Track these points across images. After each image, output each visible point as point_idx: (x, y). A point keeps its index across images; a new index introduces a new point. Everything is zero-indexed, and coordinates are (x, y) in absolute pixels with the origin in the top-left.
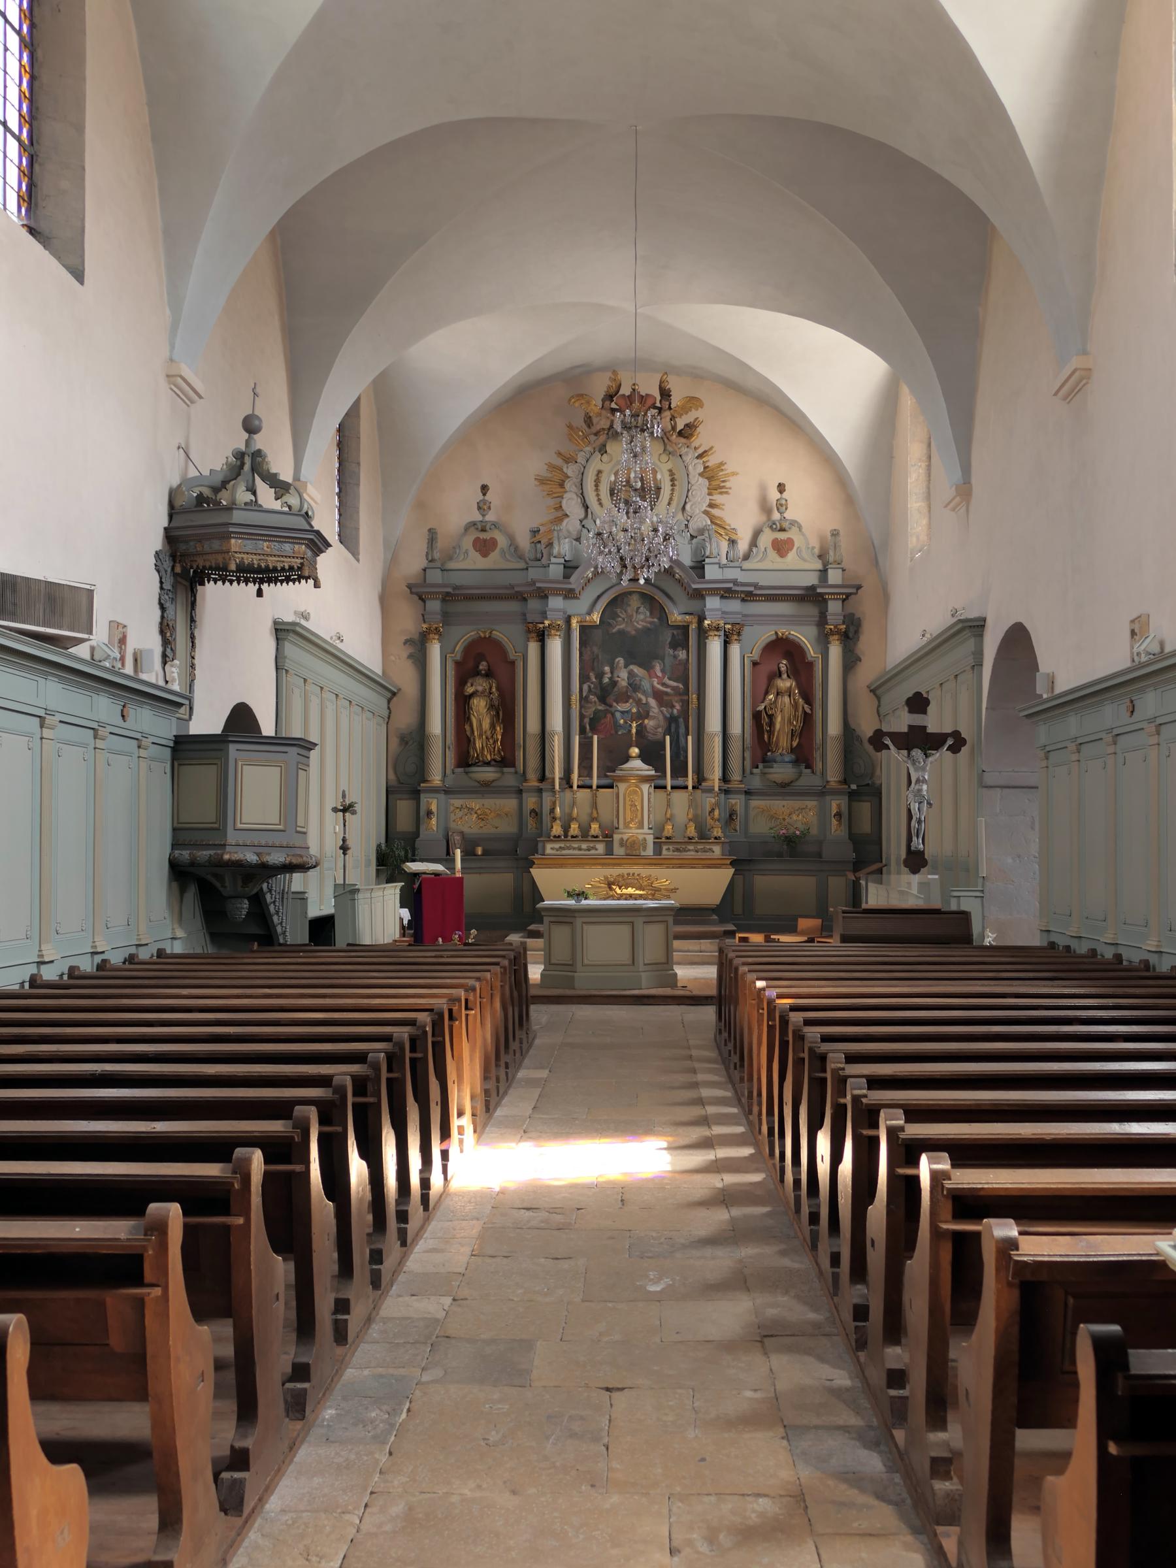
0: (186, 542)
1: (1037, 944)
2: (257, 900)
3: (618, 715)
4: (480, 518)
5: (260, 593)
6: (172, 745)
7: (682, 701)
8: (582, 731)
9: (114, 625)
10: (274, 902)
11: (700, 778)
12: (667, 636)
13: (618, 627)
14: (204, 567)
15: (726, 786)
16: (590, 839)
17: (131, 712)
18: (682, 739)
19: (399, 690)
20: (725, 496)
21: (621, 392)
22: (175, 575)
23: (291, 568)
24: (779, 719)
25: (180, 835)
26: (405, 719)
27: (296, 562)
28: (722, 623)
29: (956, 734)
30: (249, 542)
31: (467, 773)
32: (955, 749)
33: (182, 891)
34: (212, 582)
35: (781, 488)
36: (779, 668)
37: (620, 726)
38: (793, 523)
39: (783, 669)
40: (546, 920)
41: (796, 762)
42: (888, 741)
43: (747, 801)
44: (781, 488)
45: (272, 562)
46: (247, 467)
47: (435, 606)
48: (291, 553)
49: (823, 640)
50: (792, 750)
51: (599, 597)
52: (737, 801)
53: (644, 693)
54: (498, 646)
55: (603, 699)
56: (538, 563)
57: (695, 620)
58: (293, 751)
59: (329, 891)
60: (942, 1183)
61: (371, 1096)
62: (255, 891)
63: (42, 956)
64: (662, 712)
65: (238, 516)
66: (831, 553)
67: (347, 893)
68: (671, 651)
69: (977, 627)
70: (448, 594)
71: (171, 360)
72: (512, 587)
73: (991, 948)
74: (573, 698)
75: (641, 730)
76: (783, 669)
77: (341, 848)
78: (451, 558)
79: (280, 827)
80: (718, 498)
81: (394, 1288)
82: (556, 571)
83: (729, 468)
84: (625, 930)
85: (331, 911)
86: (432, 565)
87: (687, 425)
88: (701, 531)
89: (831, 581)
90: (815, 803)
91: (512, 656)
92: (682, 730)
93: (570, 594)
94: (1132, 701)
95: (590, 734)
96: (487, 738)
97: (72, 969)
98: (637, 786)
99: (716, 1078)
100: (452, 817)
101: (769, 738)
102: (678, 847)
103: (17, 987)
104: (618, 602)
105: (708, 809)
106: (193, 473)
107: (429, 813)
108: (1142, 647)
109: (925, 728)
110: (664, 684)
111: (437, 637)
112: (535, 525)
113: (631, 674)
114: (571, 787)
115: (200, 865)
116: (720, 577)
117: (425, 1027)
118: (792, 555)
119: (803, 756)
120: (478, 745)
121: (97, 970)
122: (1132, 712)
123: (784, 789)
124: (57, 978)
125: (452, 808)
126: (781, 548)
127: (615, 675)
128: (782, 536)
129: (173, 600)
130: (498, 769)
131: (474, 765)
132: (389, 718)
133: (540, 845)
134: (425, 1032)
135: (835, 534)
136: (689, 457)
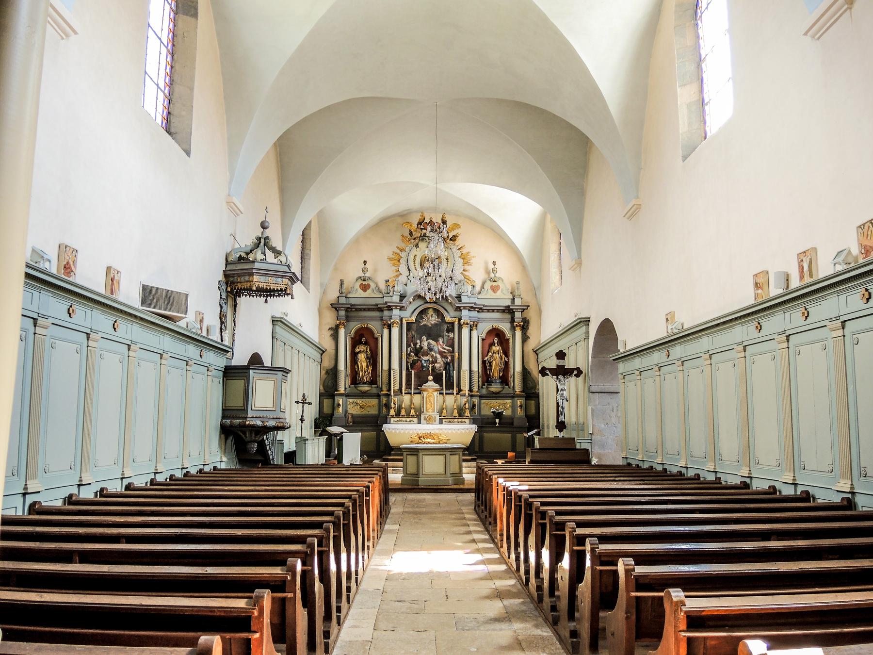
0: (233, 277)
1: (621, 464)
2: (262, 444)
3: (423, 362)
4: (363, 275)
5: (266, 301)
6: (223, 370)
7: (452, 355)
8: (407, 368)
9: (198, 313)
10: (269, 444)
11: (460, 390)
12: (445, 327)
13: (423, 323)
14: (241, 288)
15: (471, 394)
16: (410, 417)
17: (204, 354)
18: (451, 372)
19: (326, 350)
20: (470, 266)
21: (425, 221)
22: (228, 292)
23: (281, 290)
24: (494, 364)
25: (226, 412)
26: (328, 363)
27: (283, 287)
28: (469, 321)
29: (578, 369)
30: (262, 277)
31: (356, 387)
32: (578, 376)
33: (226, 439)
34: (244, 296)
35: (494, 263)
36: (494, 341)
37: (424, 367)
38: (500, 278)
39: (496, 342)
40: (405, 454)
41: (502, 383)
42: (548, 372)
43: (480, 400)
44: (494, 263)
45: (272, 287)
46: (262, 244)
47: (342, 313)
48: (281, 283)
49: (513, 329)
50: (500, 378)
51: (415, 310)
52: (476, 400)
53: (435, 352)
54: (370, 331)
55: (416, 355)
56: (388, 295)
57: (457, 320)
58: (280, 373)
59: (294, 440)
60: (681, 608)
61: (325, 547)
62: (261, 439)
63: (157, 470)
64: (442, 360)
65: (257, 265)
66: (516, 291)
67: (301, 441)
68: (447, 334)
69: (586, 321)
70: (348, 308)
71: (229, 195)
72: (377, 305)
73: (595, 466)
74: (403, 354)
75: (434, 368)
76: (496, 342)
77: (300, 420)
78: (350, 293)
79: (273, 409)
80: (467, 267)
81: (335, 650)
82: (396, 299)
83: (472, 254)
84: (442, 458)
85: (295, 449)
86: (342, 295)
87: (454, 236)
88: (460, 282)
89: (516, 303)
90: (510, 401)
91: (376, 335)
92: (451, 369)
93: (402, 308)
94: (668, 351)
95: (411, 370)
96: (365, 371)
97: (171, 476)
98: (432, 393)
99: (479, 529)
100: (349, 407)
101: (489, 372)
102: (450, 420)
103: (144, 485)
104: (423, 312)
105: (463, 404)
106: (237, 246)
107: (339, 405)
108: (674, 326)
109: (564, 366)
110: (443, 348)
111: (343, 327)
112: (387, 279)
113: (429, 344)
114: (402, 393)
115: (235, 427)
116: (468, 301)
117: (349, 507)
118: (499, 292)
119: (505, 380)
120: (361, 374)
121: (184, 476)
122: (669, 356)
123: (496, 395)
124: (164, 481)
125: (349, 403)
126: (494, 289)
127: (422, 344)
128: (495, 284)
129: (226, 303)
130: (370, 385)
131: (359, 384)
132: (321, 362)
133: (388, 420)
134: (349, 510)
135: (518, 283)
136: (455, 249)
